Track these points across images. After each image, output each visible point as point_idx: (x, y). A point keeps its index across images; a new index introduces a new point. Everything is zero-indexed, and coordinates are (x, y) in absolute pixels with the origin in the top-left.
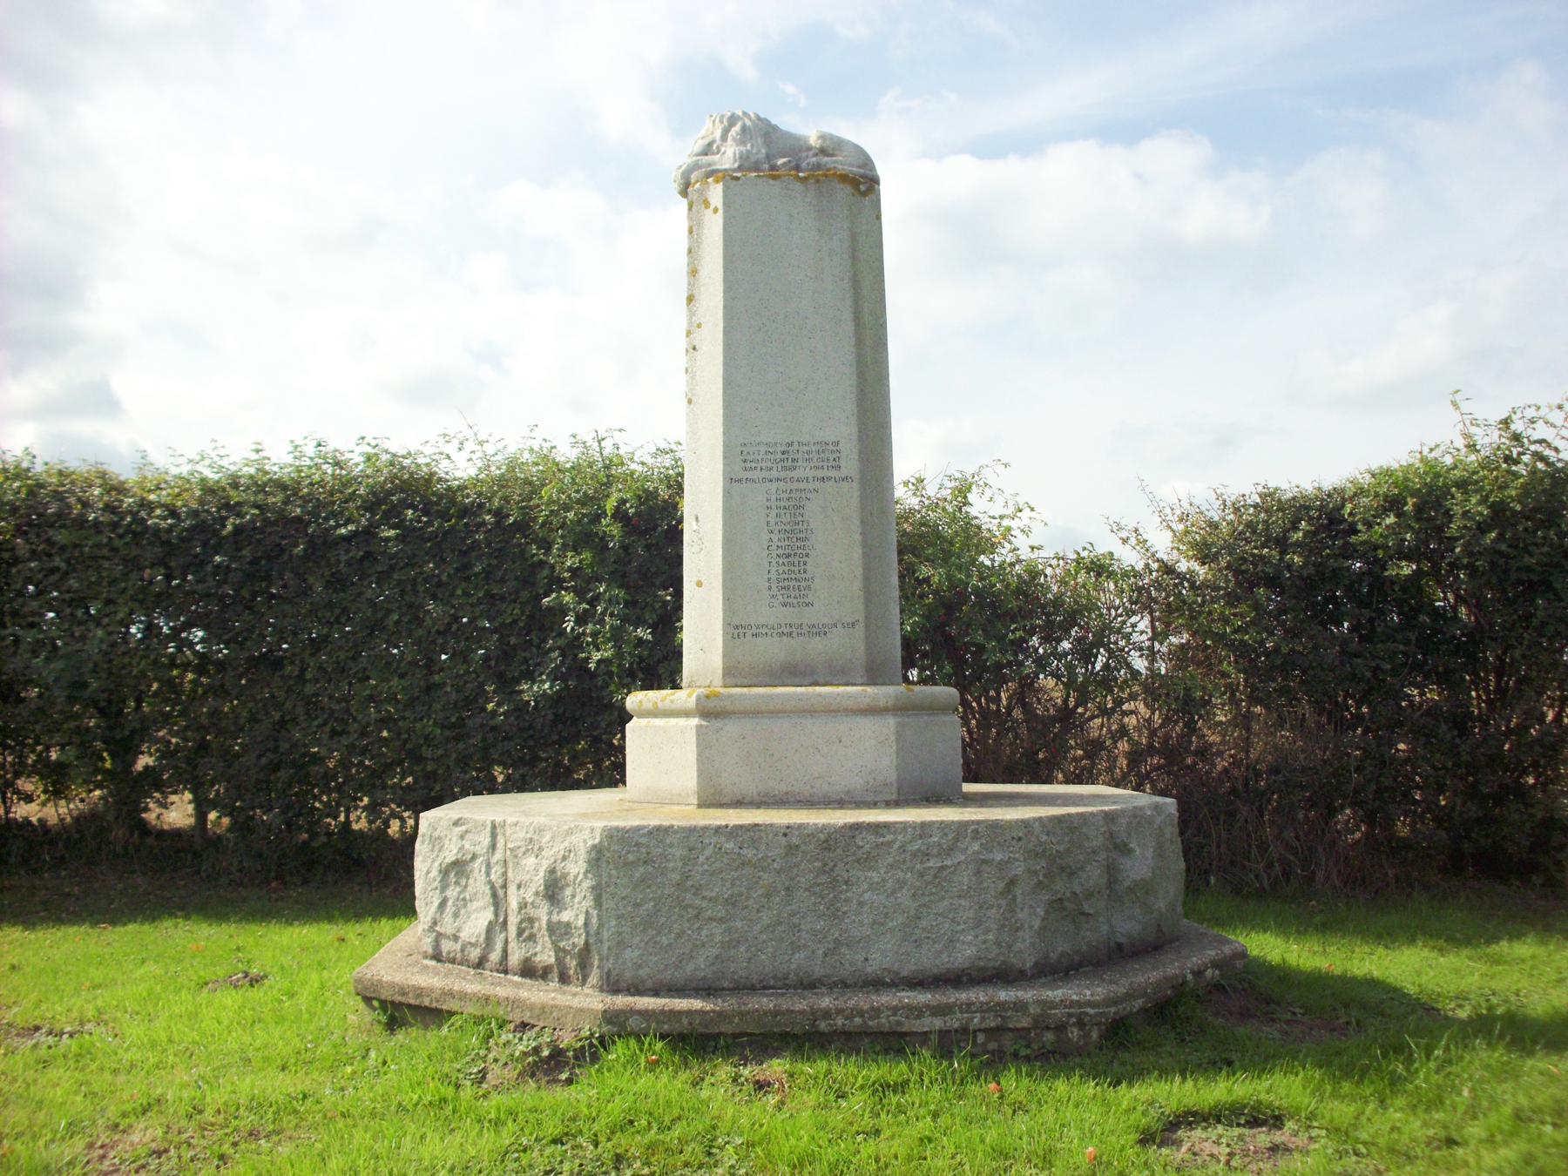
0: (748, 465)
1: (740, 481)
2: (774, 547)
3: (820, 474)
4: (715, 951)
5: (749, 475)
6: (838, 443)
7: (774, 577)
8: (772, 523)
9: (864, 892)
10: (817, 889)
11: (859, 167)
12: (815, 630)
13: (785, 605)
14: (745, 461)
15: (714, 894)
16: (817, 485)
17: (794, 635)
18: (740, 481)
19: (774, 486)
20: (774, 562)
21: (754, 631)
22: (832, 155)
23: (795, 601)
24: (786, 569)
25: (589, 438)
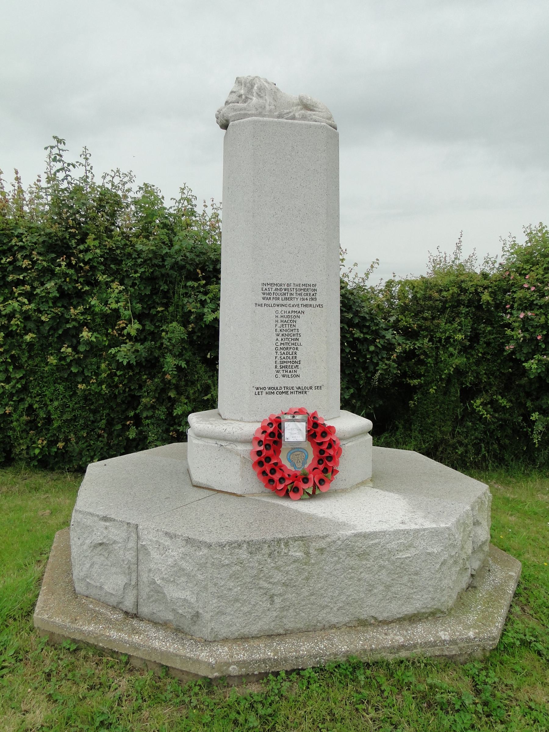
0: (265, 296)
1: (261, 305)
2: (279, 344)
3: (305, 302)
4: (275, 614)
5: (267, 302)
6: (315, 285)
7: (278, 361)
8: (278, 329)
9: (361, 573)
10: (335, 573)
11: (328, 119)
12: (300, 390)
13: (284, 376)
14: (264, 294)
15: (276, 581)
16: (303, 309)
17: (289, 393)
18: (261, 305)
19: (280, 309)
20: (279, 353)
21: (267, 390)
22: (311, 110)
23: (290, 374)
24: (285, 356)
25: (505, 237)
